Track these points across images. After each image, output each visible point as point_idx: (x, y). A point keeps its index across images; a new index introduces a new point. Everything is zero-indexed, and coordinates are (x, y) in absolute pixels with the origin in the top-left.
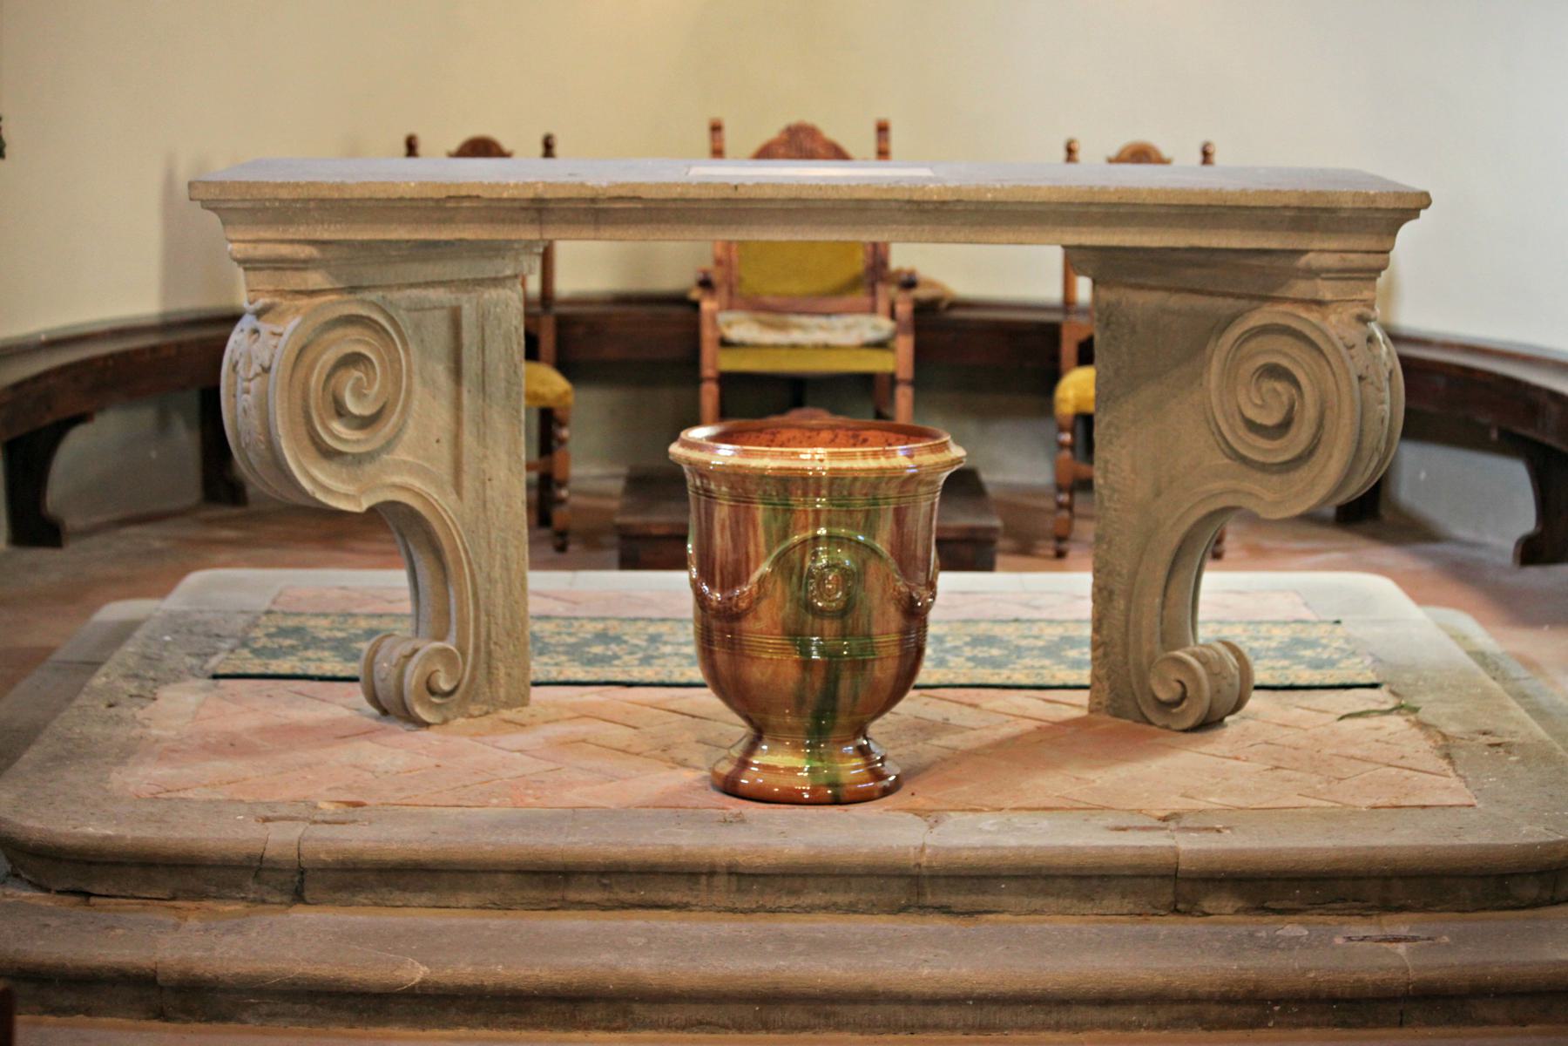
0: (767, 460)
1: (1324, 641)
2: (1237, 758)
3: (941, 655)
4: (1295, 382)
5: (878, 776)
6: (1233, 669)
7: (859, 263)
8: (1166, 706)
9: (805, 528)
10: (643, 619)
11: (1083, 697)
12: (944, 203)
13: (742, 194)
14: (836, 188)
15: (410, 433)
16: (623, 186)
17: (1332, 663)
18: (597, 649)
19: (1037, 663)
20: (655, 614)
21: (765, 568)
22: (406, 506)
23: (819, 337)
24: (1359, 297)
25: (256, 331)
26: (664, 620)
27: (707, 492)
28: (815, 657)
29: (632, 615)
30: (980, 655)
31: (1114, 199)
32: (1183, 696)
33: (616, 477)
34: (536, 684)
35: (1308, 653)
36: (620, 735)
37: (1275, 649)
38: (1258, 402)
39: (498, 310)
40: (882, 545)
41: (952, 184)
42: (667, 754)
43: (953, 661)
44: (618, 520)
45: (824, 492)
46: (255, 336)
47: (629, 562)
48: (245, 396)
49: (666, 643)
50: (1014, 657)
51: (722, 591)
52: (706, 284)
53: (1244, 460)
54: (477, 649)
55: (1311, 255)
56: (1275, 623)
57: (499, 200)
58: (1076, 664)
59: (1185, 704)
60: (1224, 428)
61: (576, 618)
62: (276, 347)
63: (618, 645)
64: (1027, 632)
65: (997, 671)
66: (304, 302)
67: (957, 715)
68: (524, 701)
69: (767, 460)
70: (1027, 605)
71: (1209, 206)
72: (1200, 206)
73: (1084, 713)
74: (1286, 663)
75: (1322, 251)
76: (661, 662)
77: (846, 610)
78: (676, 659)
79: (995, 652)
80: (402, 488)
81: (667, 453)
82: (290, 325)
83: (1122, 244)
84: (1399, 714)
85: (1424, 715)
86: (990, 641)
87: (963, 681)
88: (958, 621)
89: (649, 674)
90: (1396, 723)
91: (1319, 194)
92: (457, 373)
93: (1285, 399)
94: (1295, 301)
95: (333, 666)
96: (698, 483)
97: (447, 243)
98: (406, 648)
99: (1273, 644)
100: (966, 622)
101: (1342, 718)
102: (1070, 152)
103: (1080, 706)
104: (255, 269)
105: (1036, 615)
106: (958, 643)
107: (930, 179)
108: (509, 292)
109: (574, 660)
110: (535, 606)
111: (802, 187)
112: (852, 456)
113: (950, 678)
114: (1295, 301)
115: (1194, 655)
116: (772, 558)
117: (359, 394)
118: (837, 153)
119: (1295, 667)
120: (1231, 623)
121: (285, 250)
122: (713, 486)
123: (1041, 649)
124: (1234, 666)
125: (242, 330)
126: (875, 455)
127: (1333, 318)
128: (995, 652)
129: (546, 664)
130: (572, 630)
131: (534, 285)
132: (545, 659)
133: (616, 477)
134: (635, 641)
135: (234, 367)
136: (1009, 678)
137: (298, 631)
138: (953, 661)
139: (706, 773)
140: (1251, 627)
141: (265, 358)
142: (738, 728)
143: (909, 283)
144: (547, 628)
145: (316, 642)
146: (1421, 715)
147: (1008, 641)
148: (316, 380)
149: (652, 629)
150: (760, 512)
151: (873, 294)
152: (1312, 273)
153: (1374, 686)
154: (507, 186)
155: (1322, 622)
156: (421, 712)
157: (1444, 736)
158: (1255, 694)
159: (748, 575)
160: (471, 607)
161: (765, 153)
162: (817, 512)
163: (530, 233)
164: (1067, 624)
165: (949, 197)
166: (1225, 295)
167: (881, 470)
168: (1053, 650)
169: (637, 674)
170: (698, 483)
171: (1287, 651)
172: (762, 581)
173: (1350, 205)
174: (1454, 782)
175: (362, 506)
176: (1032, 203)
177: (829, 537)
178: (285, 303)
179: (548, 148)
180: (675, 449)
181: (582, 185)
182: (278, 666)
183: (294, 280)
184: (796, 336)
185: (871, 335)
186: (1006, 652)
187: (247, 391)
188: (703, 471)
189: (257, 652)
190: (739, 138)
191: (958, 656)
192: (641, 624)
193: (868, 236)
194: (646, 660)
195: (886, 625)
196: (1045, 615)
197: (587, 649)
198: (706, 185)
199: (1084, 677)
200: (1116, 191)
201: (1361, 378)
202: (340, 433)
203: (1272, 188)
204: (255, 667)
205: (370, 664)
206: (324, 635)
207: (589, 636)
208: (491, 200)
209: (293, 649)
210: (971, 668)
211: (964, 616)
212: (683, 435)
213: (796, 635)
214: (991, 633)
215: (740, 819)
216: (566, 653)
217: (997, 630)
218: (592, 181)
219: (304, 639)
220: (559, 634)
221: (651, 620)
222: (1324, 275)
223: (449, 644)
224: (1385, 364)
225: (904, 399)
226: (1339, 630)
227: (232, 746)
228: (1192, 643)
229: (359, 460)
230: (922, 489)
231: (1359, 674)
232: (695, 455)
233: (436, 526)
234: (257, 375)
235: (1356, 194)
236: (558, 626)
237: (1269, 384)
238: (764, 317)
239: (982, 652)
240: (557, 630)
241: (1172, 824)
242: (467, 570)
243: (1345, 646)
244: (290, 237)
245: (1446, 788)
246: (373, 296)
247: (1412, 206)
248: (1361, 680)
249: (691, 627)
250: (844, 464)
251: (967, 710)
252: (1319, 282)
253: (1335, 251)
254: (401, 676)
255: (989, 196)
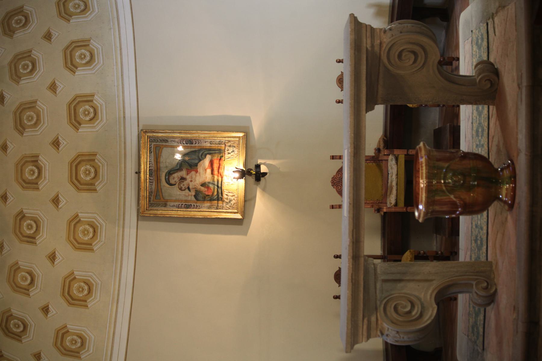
0: (423, 196)
1: (477, 36)
2: (505, 66)
3: (481, 146)
4: (403, 50)
5: (509, 166)
6: (482, 66)
7: (373, 165)
8: (492, 85)
9: (441, 186)
10: (471, 230)
11: (491, 107)
12: (354, 147)
13: (352, 202)
14: (350, 176)
15: (416, 294)
16: (349, 234)
17: (482, 35)
18: (479, 242)
19: (483, 119)
20: (470, 226)
21: (452, 197)
22: (436, 295)
23: (394, 177)
24: (379, 33)
25: (387, 335)
26: (472, 223)
27: (432, 212)
28: (476, 183)
29: (470, 232)
30: (481, 134)
31: (353, 101)
32: (489, 80)
33: (436, 237)
34: (487, 259)
35: (480, 41)
36: (499, 236)
37: (479, 50)
38: (408, 60)
39: (177, 181)
40: (446, 165)
41: (349, 145)
42: (504, 223)
43: (482, 142)
44: (447, 237)
45: (432, 181)
46: (389, 336)
47: (458, 234)
48: (405, 338)
49: (478, 223)
50: (481, 125)
51: (458, 208)
52: (378, 210)
53: (424, 64)
54: (476, 276)
55: (368, 46)
56: (472, 50)
57: (353, 268)
58: (483, 108)
59: (491, 80)
60: (415, 69)
61: (471, 248)
62: (391, 330)
63: (478, 236)
64: (475, 120)
65: (485, 130)
66: (379, 322)
67: (495, 143)
68: (491, 262)
69: (423, 196)
70: (469, 120)
71: (355, 75)
72: (355, 78)
73: (495, 107)
74: (482, 48)
75: (366, 43)
76: (482, 224)
77: (464, 175)
78: (482, 220)
79: (480, 130)
80: (431, 295)
81: (421, 223)
82: (386, 326)
83: (365, 99)
84: (494, 18)
85: (494, 11)
86: (477, 131)
87: (487, 140)
88: (472, 140)
89: (485, 228)
90: (496, 19)
91: (351, 44)
92: (400, 281)
93: (407, 53)
94: (380, 50)
95: (481, 317)
96: (429, 215)
97: (364, 283)
98: (475, 295)
99: (478, 51)
100: (473, 138)
101: (495, 35)
102: (339, 102)
103: (493, 108)
104: (370, 335)
105: (471, 117)
106: (478, 140)
107: (348, 151)
108: (378, 266)
109: (481, 249)
110: (468, 259)
111: (350, 186)
112: (422, 173)
113: (486, 143)
114: (380, 50)
115: (478, 77)
116: (449, 195)
117: (405, 307)
118: (340, 171)
119: (483, 46)
120: (473, 62)
121: (365, 327)
122: (430, 211)
123: (479, 117)
124: (481, 66)
125: (387, 339)
126: (422, 167)
127: (385, 40)
128: (480, 130)
129: (482, 257)
130: (474, 249)
131: (379, 261)
132: (481, 257)
133: (436, 237)
134: (477, 231)
135: (396, 341)
136: (486, 127)
137: (473, 327)
138: (482, 142)
139: (508, 213)
140: (474, 57)
141: (394, 333)
142: (496, 204)
143: (378, 150)
144: (473, 256)
145: (476, 322)
146: (494, 12)
147: (478, 126)
148: (401, 319)
149: (474, 227)
150: (437, 198)
151: (382, 160)
152: (373, 46)
153: (487, 24)
154: (349, 266)
155: (472, 36)
156: (492, 291)
157: (499, 7)
158: (490, 60)
159: (454, 201)
160: (464, 277)
161: (340, 193)
162: (437, 182)
163: (362, 260)
164: (473, 109)
165: (353, 146)
166: (379, 69)
167: (426, 165)
168: (480, 114)
169: (485, 231)
170: (429, 215)
171: (479, 47)
172: (455, 197)
173: (354, 36)
174: (510, 7)
175: (435, 307)
176: (354, 123)
177: (444, 179)
178: (380, 327)
179: (338, 257)
180: (421, 220)
181: (349, 246)
182: (481, 333)
183: (373, 325)
184: (394, 184)
185: (394, 162)
186: (480, 127)
187: (403, 338)
188: (426, 213)
189: (478, 338)
190: (335, 200)
191: (481, 141)
192: (473, 230)
193: (363, 163)
194: (482, 229)
195: (469, 164)
196: (471, 115)
197: (479, 245)
198: (349, 212)
199: (486, 107)
200: (351, 100)
201: (401, 33)
202: (415, 312)
203: (350, 57)
204: (481, 339)
205: (479, 305)
206: (474, 320)
207: (476, 245)
208: (353, 270)
209: (477, 328)
210: (484, 138)
211: (471, 138)
212: (417, 218)
213: (470, 188)
214: (475, 131)
215: (519, 203)
216: (480, 251)
217: (475, 129)
218: (348, 243)
219: (475, 325)
220: (475, 253)
221: (472, 227)
222: (373, 43)
223: (474, 283)
224: (397, 25)
225: (412, 152)
226: (474, 31)
227: (500, 343)
228: (475, 77)
229: (423, 307)
230: (431, 154)
231: (485, 28)
232: (422, 215)
233: (442, 287)
234: (399, 335)
235: (351, 34)
236: (473, 254)
237: (403, 58)
238: (388, 193)
239: (480, 134)
240: (474, 254)
241: (520, 86)
242: (454, 278)
243: (478, 30)
244: (361, 325)
245: (511, 9)
246: (378, 303)
247: (353, 18)
248: (486, 28)
249: (474, 216)
250: (424, 175)
251: (494, 139)
252: (375, 44)
253: (366, 39)
254: (483, 296)
255: (352, 135)
